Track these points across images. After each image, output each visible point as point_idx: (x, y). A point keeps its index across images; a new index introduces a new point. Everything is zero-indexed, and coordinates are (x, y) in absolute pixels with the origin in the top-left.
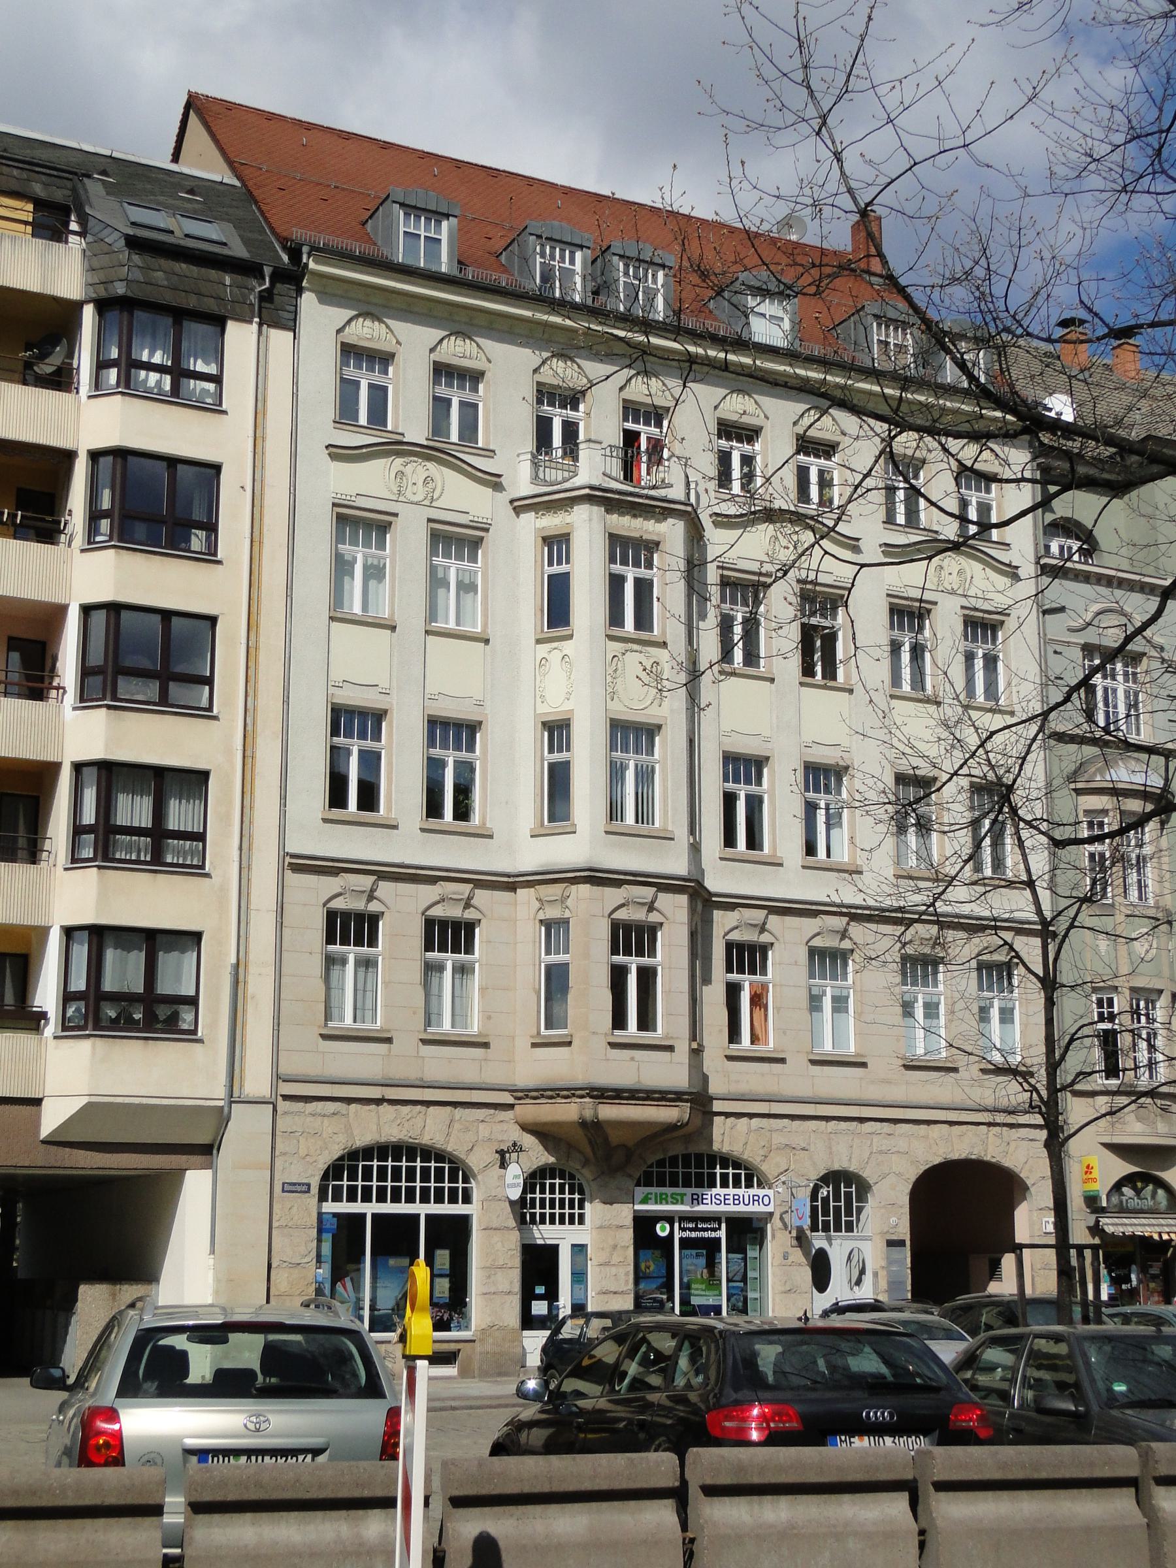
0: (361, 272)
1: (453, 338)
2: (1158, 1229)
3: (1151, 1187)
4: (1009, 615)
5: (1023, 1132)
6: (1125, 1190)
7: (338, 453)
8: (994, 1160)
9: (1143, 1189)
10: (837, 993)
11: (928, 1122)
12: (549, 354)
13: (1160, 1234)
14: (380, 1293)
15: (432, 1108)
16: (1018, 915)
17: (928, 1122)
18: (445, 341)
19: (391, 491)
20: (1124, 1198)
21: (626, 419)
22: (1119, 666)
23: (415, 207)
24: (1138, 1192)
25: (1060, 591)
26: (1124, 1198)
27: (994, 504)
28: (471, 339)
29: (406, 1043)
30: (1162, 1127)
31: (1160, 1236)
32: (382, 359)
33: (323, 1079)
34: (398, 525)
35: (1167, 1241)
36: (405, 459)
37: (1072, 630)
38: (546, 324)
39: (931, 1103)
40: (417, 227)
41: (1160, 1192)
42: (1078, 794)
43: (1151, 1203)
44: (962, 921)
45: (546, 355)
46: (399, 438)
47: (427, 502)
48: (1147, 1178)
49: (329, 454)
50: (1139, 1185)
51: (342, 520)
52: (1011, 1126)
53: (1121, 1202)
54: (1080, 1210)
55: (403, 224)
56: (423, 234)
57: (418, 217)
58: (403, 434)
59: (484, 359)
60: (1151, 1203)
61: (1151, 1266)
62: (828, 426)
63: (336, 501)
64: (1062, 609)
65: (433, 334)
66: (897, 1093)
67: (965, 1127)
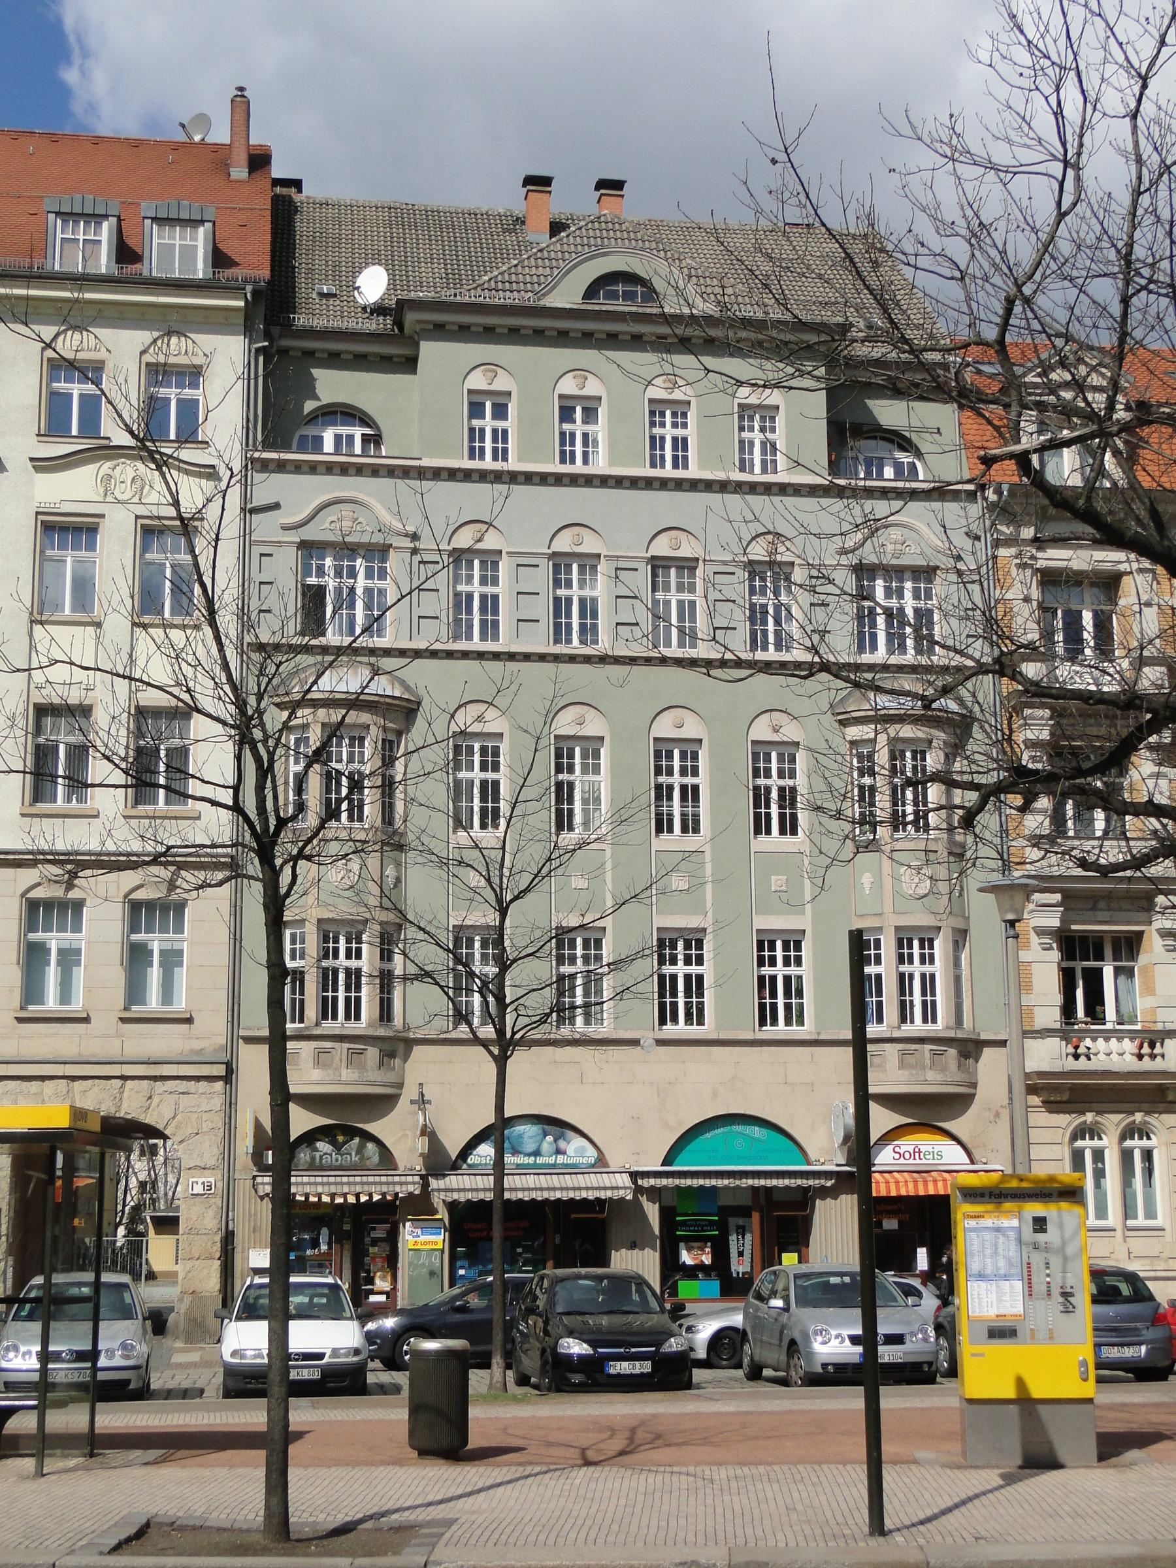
0: (99, 292)
1: (69, 333)
2: (333, 1189)
3: (357, 1140)
4: (202, 519)
5: (170, 1085)
6: (321, 1145)
7: (42, 465)
8: (129, 1117)
9: (345, 1143)
10: (65, 945)
11: (43, 1078)
12: (1015, 368)
13: (357, 1196)
14: (438, 1261)
15: (47, 1082)
16: (124, 848)
17: (43, 1078)
18: (61, 338)
19: (99, 495)
20: (317, 1154)
21: (52, 379)
22: (328, 562)
23: (71, 214)
24: (338, 1147)
25: (267, 488)
26: (317, 1154)
27: (201, 398)
28: (185, 336)
29: (105, 1020)
30: (347, 1074)
31: (333, 1199)
32: (193, 374)
33: (136, 1060)
34: (105, 526)
35: (314, 1204)
36: (114, 462)
37: (286, 528)
38: (27, 298)
39: (51, 1057)
40: (172, 238)
41: (370, 1146)
42: (845, 726)
43: (355, 1158)
44: (79, 858)
45: (156, 334)
46: (106, 442)
47: (136, 500)
48: (352, 1132)
49: (34, 467)
50: (340, 1138)
51: (48, 528)
52: (155, 1078)
53: (313, 1158)
54: (245, 1168)
55: (59, 231)
56: (81, 237)
57: (76, 222)
58: (108, 438)
59: (103, 350)
60: (355, 1158)
61: (374, 1229)
62: (177, 350)
63: (40, 510)
64: (276, 506)
65: (143, 337)
66: (112, 1050)
67: (90, 1082)
